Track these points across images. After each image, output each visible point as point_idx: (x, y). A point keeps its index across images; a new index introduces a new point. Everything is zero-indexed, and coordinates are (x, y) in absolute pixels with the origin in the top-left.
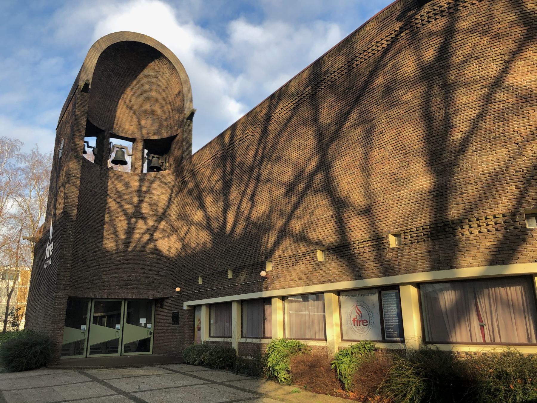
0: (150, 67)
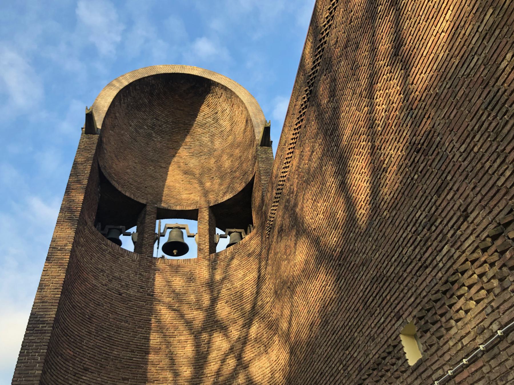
0: (203, 111)
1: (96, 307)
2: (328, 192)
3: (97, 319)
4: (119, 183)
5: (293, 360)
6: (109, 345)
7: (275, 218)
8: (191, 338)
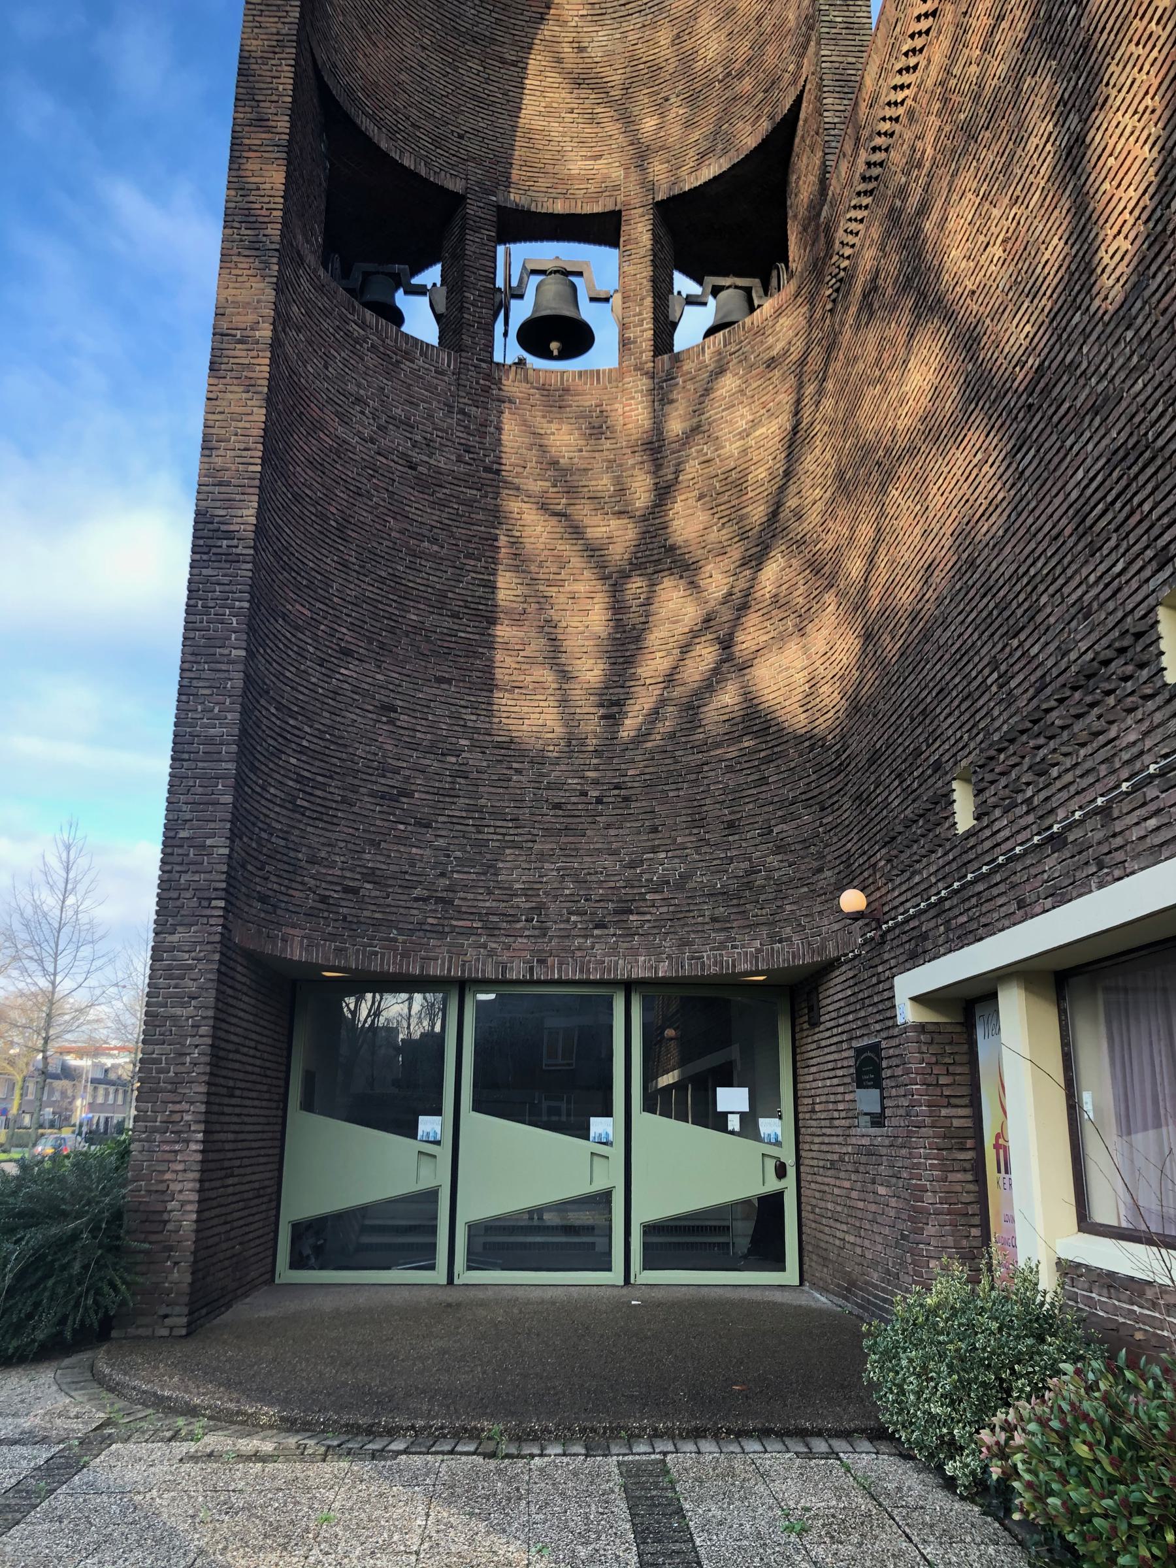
1: (351, 500)
2: (1028, 170)
3: (359, 530)
4: (379, 123)
5: (870, 655)
6: (395, 598)
7: (857, 248)
8: (604, 588)
